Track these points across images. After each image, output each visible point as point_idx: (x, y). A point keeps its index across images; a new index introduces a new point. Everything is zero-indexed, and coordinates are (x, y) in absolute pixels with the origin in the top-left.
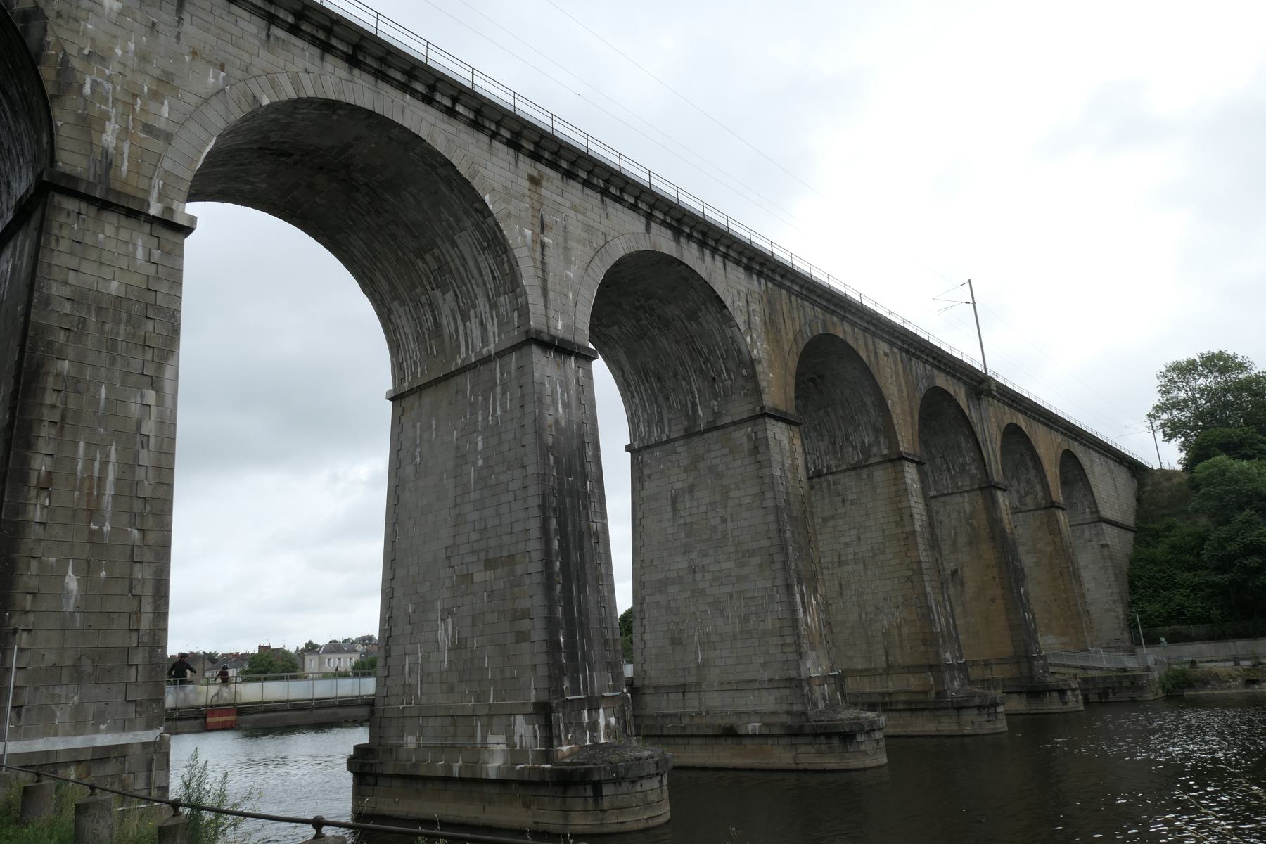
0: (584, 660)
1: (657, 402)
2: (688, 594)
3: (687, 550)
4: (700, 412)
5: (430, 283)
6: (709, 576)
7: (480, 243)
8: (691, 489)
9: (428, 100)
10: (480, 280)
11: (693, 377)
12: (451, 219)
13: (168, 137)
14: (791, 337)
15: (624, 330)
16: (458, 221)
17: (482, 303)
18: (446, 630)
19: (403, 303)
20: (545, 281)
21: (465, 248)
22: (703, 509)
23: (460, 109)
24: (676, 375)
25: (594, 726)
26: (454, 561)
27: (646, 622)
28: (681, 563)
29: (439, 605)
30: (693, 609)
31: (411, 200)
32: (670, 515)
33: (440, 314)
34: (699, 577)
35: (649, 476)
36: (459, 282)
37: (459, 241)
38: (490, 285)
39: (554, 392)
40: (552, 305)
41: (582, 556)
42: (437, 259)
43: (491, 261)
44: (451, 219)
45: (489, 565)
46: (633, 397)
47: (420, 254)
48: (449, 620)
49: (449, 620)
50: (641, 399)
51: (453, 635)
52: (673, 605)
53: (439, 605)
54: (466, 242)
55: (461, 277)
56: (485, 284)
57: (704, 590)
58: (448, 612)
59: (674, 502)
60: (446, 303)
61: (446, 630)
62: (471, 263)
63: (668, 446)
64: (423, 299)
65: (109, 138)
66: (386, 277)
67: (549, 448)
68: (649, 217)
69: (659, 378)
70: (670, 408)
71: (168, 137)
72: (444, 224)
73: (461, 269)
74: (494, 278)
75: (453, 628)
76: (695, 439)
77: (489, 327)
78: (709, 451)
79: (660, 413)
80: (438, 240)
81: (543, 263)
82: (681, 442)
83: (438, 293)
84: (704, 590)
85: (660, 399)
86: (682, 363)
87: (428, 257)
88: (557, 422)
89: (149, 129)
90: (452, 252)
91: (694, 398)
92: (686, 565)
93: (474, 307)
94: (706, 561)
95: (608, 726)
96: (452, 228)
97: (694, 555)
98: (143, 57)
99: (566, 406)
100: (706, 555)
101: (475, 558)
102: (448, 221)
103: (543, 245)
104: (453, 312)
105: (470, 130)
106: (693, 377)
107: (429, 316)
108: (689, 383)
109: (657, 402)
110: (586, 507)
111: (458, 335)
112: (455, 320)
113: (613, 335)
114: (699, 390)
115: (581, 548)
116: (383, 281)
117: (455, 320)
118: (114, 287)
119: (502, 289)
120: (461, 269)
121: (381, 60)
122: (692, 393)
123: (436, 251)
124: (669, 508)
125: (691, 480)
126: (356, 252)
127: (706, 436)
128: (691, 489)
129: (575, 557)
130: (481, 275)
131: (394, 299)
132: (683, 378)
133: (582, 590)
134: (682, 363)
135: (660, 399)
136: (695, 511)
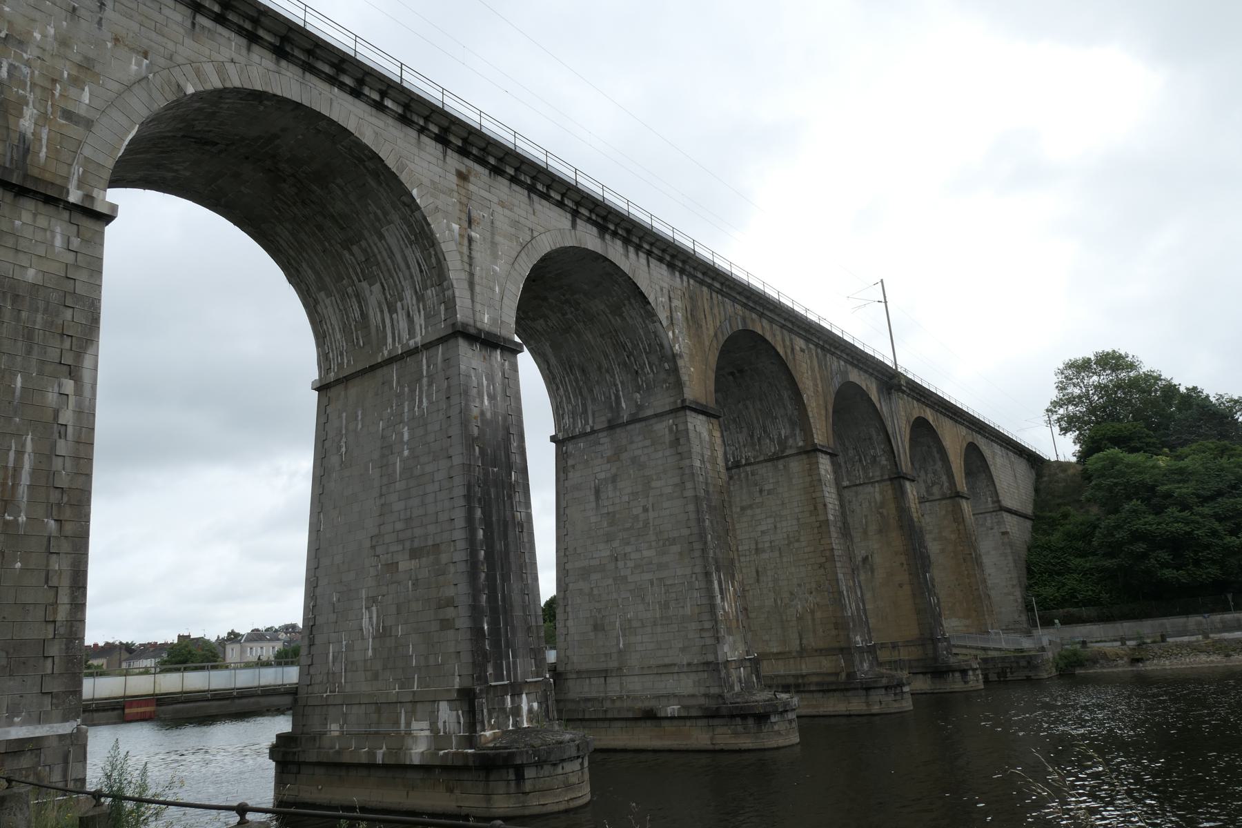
0: (508, 646)
1: (581, 393)
2: (610, 581)
3: (609, 538)
4: (624, 405)
5: (357, 274)
6: (630, 564)
7: (408, 238)
8: (614, 479)
9: (356, 93)
10: (407, 273)
11: (617, 370)
12: (379, 212)
13: (88, 124)
14: (712, 332)
15: (550, 324)
16: (385, 214)
17: (408, 294)
18: (371, 618)
19: (329, 295)
20: (472, 275)
21: (392, 241)
22: (626, 498)
23: (388, 103)
24: (600, 368)
25: (516, 711)
26: (379, 550)
27: (569, 609)
28: (604, 552)
29: (364, 594)
30: (615, 596)
31: (339, 192)
32: (594, 504)
33: (367, 305)
34: (620, 564)
35: (573, 466)
36: (387, 275)
37: (386, 234)
38: (417, 277)
39: (480, 384)
40: (478, 298)
41: (507, 545)
42: (364, 251)
43: (418, 254)
44: (379, 212)
45: (415, 554)
46: (558, 389)
47: (347, 244)
48: (374, 609)
49: (374, 609)
50: (566, 391)
51: (378, 624)
52: (595, 592)
53: (364, 594)
54: (394, 235)
55: (389, 270)
56: (412, 277)
57: (626, 577)
58: (372, 600)
59: (597, 492)
60: (373, 294)
61: (371, 618)
62: (399, 257)
63: (592, 437)
64: (350, 290)
65: (26, 123)
66: (312, 268)
67: (474, 439)
68: (575, 214)
69: (583, 371)
70: (594, 400)
71: (88, 124)
72: (372, 216)
73: (389, 261)
74: (421, 271)
75: (378, 617)
76: (618, 430)
77: (416, 319)
78: (632, 443)
79: (584, 405)
80: (366, 233)
81: (470, 257)
82: (605, 434)
83: (365, 284)
84: (626, 577)
85: (585, 391)
86: (606, 356)
87: (355, 248)
88: (482, 413)
89: (68, 115)
90: (379, 244)
91: (617, 391)
92: (608, 553)
93: (401, 300)
94: (628, 549)
95: (530, 710)
96: (379, 220)
97: (616, 544)
98: (64, 42)
99: (492, 398)
100: (628, 544)
101: (400, 547)
102: (375, 214)
103: (470, 240)
104: (379, 304)
105: (398, 124)
106: (617, 370)
107: (356, 307)
108: (613, 376)
109: (581, 393)
110: (510, 497)
111: (384, 327)
112: (382, 312)
113: (539, 328)
114: (622, 383)
115: (506, 537)
116: (310, 271)
117: (382, 312)
118: (31, 275)
119: (429, 282)
120: (389, 261)
121: (309, 52)
122: (616, 385)
123: (363, 243)
124: (592, 498)
125: (614, 471)
126: (282, 242)
127: (629, 427)
128: (614, 479)
129: (499, 546)
130: (409, 268)
131: (320, 290)
132: (607, 371)
133: (506, 578)
134: (606, 356)
135: (585, 391)
136: (617, 501)
